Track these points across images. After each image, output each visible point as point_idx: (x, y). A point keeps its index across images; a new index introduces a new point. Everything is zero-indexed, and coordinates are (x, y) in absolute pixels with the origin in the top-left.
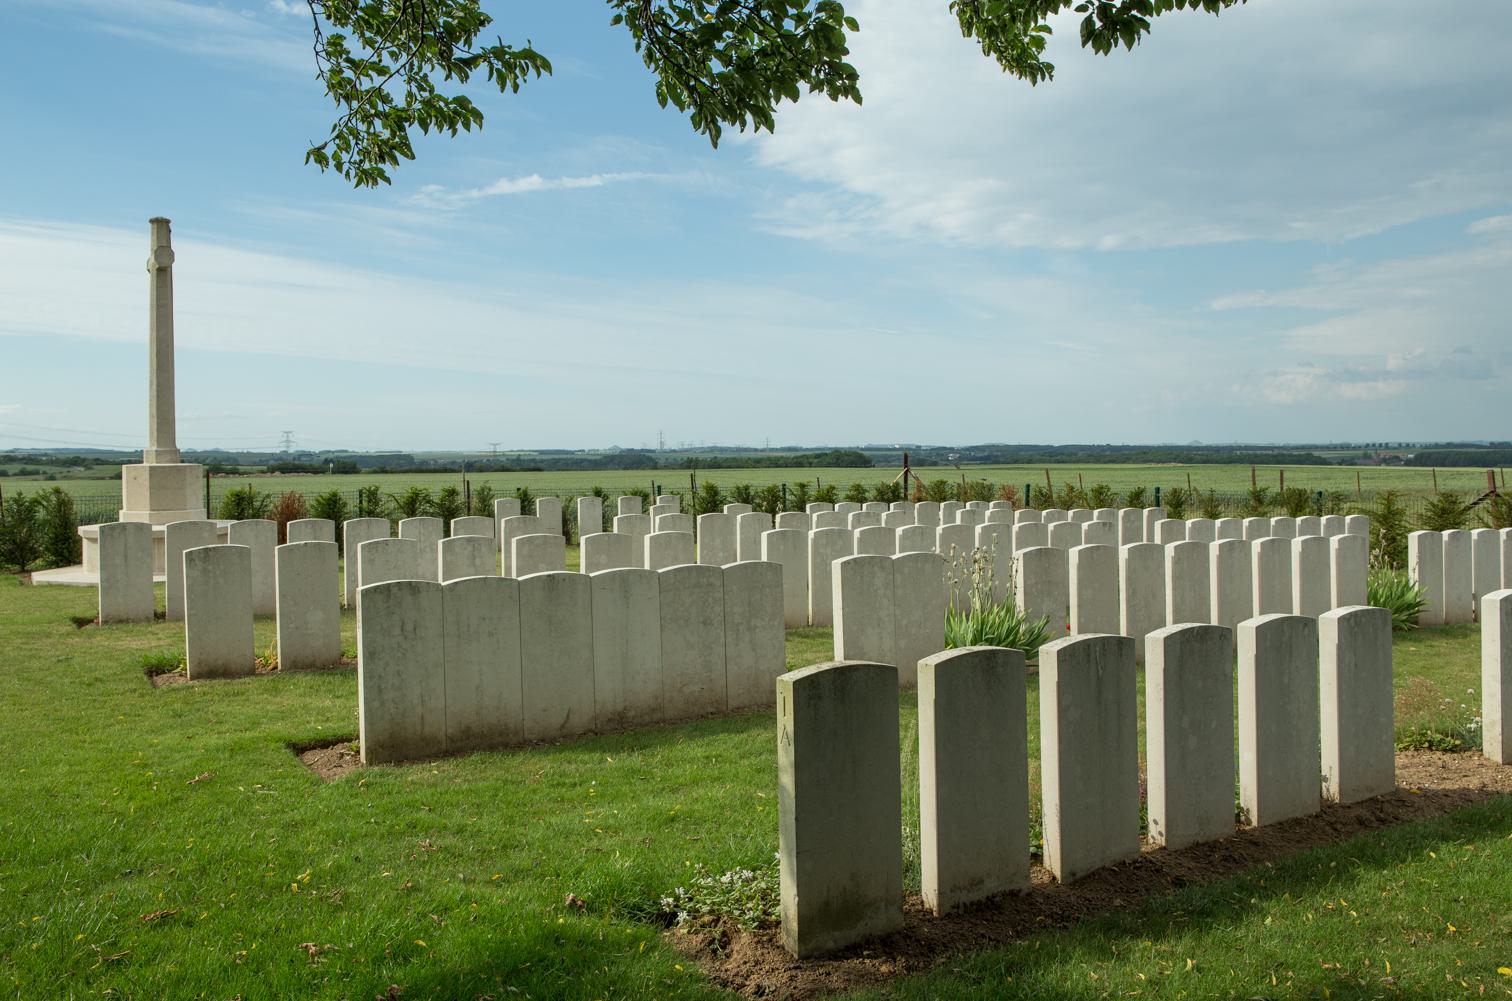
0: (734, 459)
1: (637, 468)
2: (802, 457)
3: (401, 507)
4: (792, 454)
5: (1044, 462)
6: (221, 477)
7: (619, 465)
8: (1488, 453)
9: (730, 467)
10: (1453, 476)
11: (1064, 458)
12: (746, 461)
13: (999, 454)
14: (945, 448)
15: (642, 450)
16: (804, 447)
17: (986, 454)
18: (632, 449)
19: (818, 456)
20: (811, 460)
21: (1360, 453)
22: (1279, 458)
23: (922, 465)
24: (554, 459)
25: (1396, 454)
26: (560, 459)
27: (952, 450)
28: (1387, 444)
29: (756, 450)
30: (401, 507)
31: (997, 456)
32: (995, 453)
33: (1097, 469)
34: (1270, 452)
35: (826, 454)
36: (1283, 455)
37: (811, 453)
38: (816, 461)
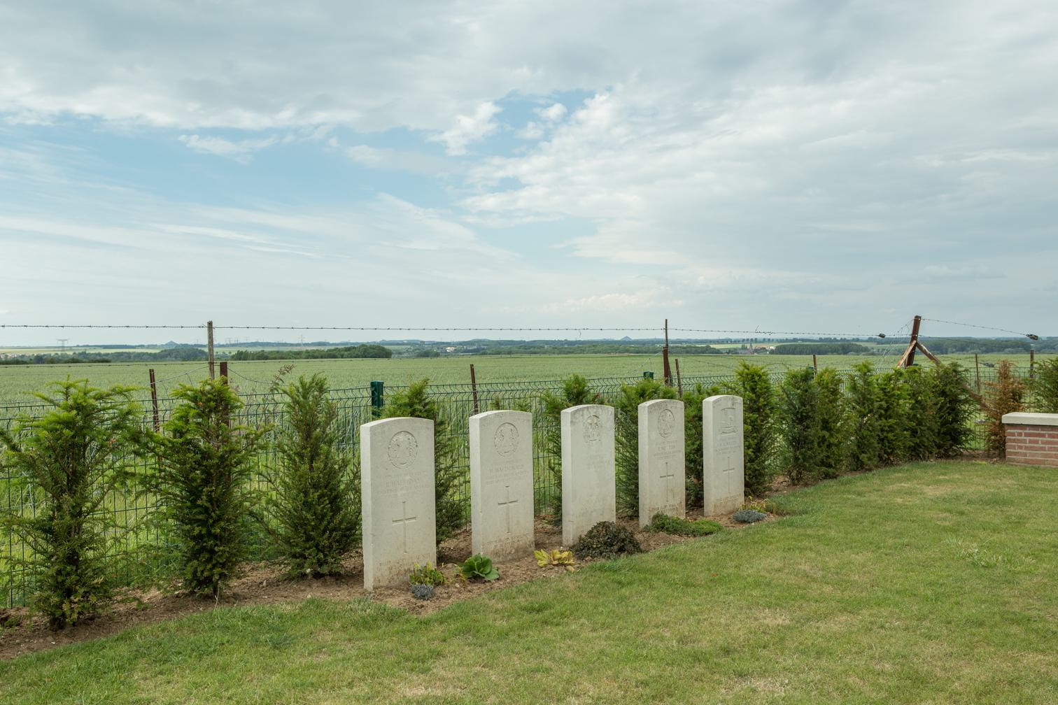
0: (278, 352)
1: (800, 354)
2: (336, 349)
3: (30, 464)
4: (326, 348)
5: (126, 362)
6: (852, 354)
7: (176, 357)
8: (821, 345)
9: (275, 358)
10: (983, 357)
11: (536, 350)
12: (289, 355)
13: (485, 347)
14: (444, 343)
15: (195, 345)
16: (331, 342)
17: (475, 347)
18: (187, 344)
19: (348, 349)
20: (342, 353)
21: (740, 346)
22: (688, 349)
23: (428, 356)
24: (118, 353)
25: (764, 347)
26: (122, 353)
27: (449, 344)
28: (756, 339)
29: (292, 345)
30: (30, 464)
31: (483, 349)
32: (483, 347)
33: (568, 358)
34: (680, 345)
35: (354, 348)
36: (691, 347)
37: (343, 347)
38: (346, 353)
